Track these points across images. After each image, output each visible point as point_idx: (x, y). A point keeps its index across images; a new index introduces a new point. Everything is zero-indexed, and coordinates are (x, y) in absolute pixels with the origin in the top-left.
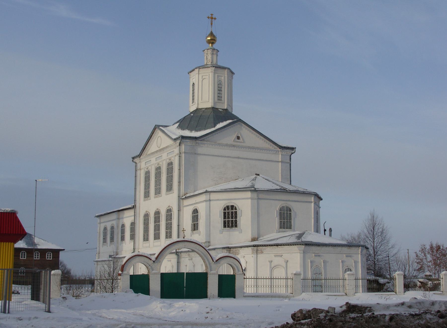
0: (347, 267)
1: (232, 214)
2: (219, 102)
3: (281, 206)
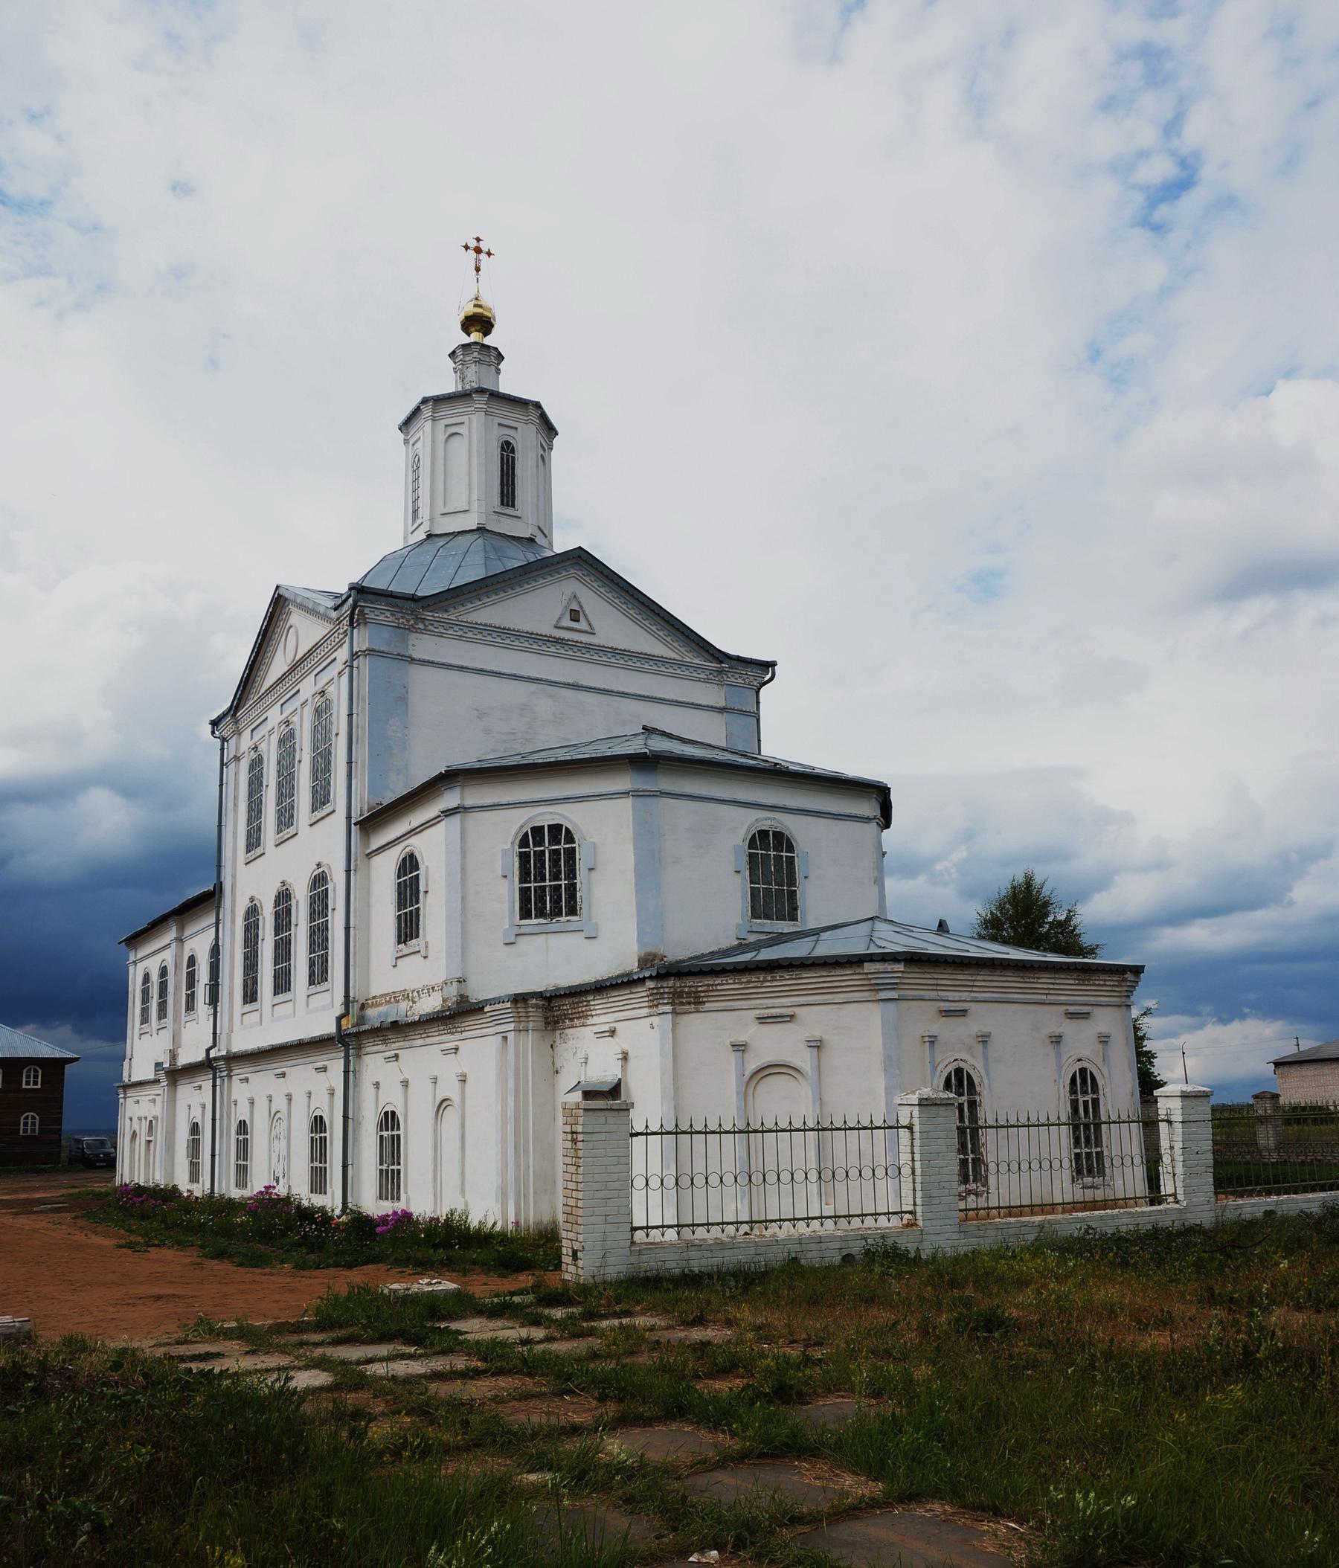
0: (1080, 1065)
1: (555, 863)
3: (753, 831)
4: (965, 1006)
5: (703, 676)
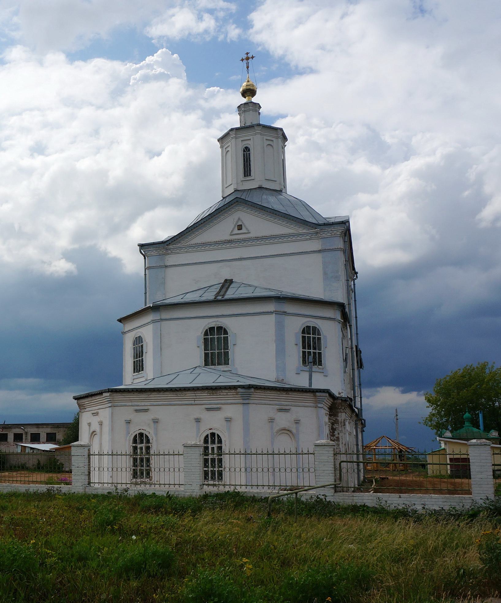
2: (246, 179)
4: (146, 408)
5: (308, 237)
